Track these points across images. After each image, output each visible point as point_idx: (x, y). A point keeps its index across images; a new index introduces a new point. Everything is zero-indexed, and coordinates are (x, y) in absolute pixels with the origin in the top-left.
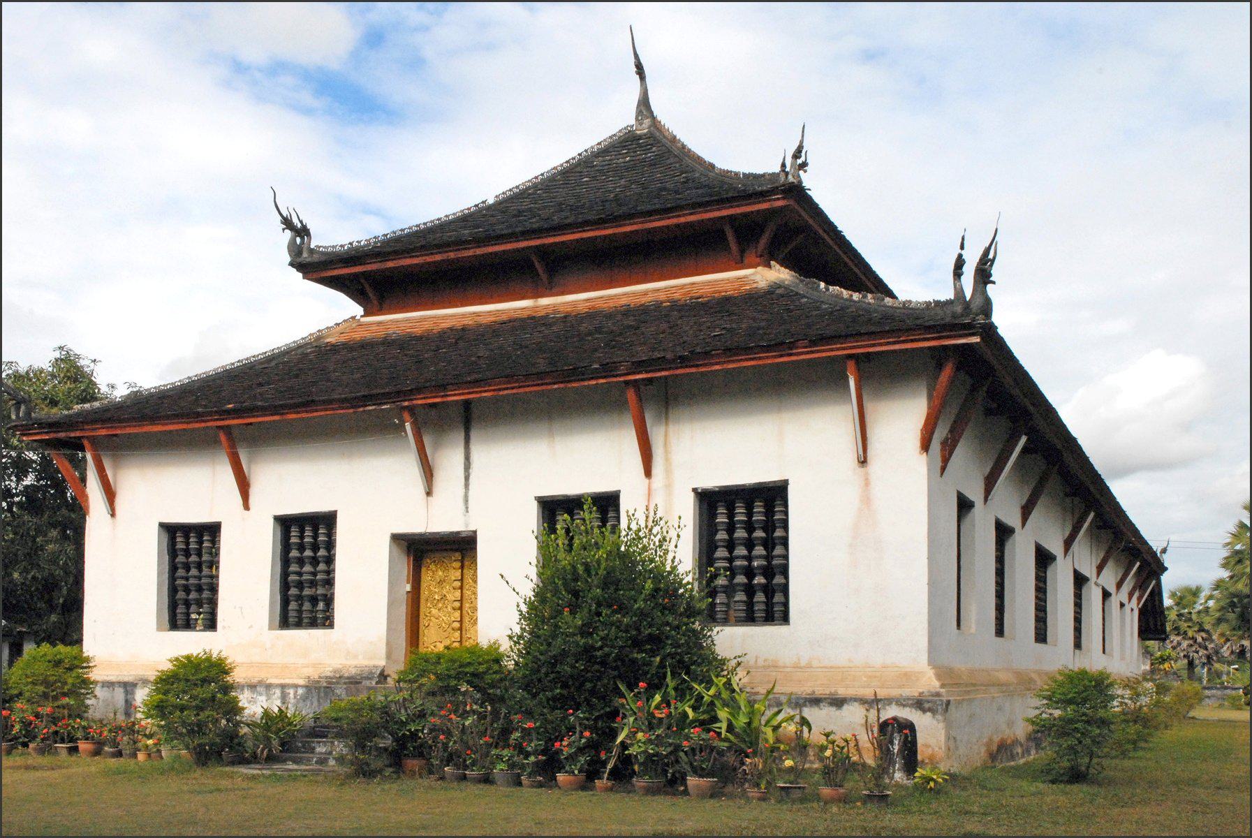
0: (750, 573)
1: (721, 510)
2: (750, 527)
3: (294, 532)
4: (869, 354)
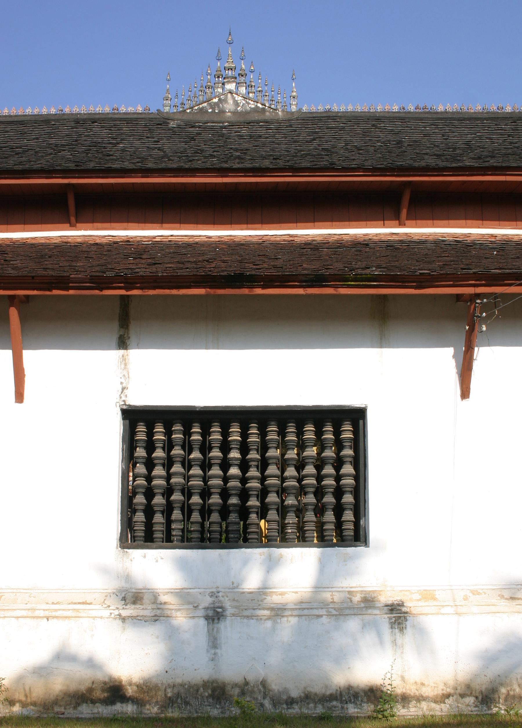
0: (187, 492)
1: (196, 429)
2: (187, 446)
3: (141, 428)
4: (385, 296)
